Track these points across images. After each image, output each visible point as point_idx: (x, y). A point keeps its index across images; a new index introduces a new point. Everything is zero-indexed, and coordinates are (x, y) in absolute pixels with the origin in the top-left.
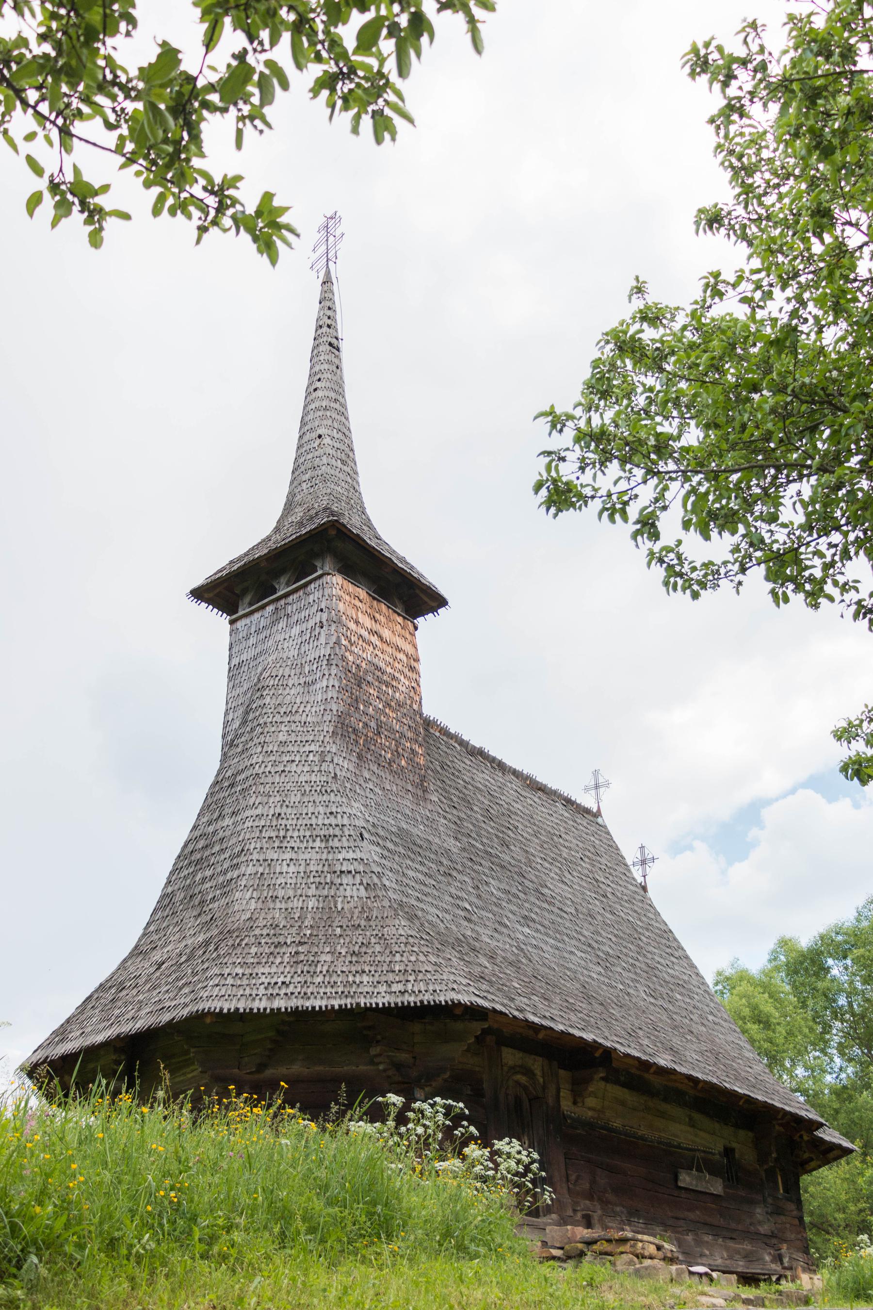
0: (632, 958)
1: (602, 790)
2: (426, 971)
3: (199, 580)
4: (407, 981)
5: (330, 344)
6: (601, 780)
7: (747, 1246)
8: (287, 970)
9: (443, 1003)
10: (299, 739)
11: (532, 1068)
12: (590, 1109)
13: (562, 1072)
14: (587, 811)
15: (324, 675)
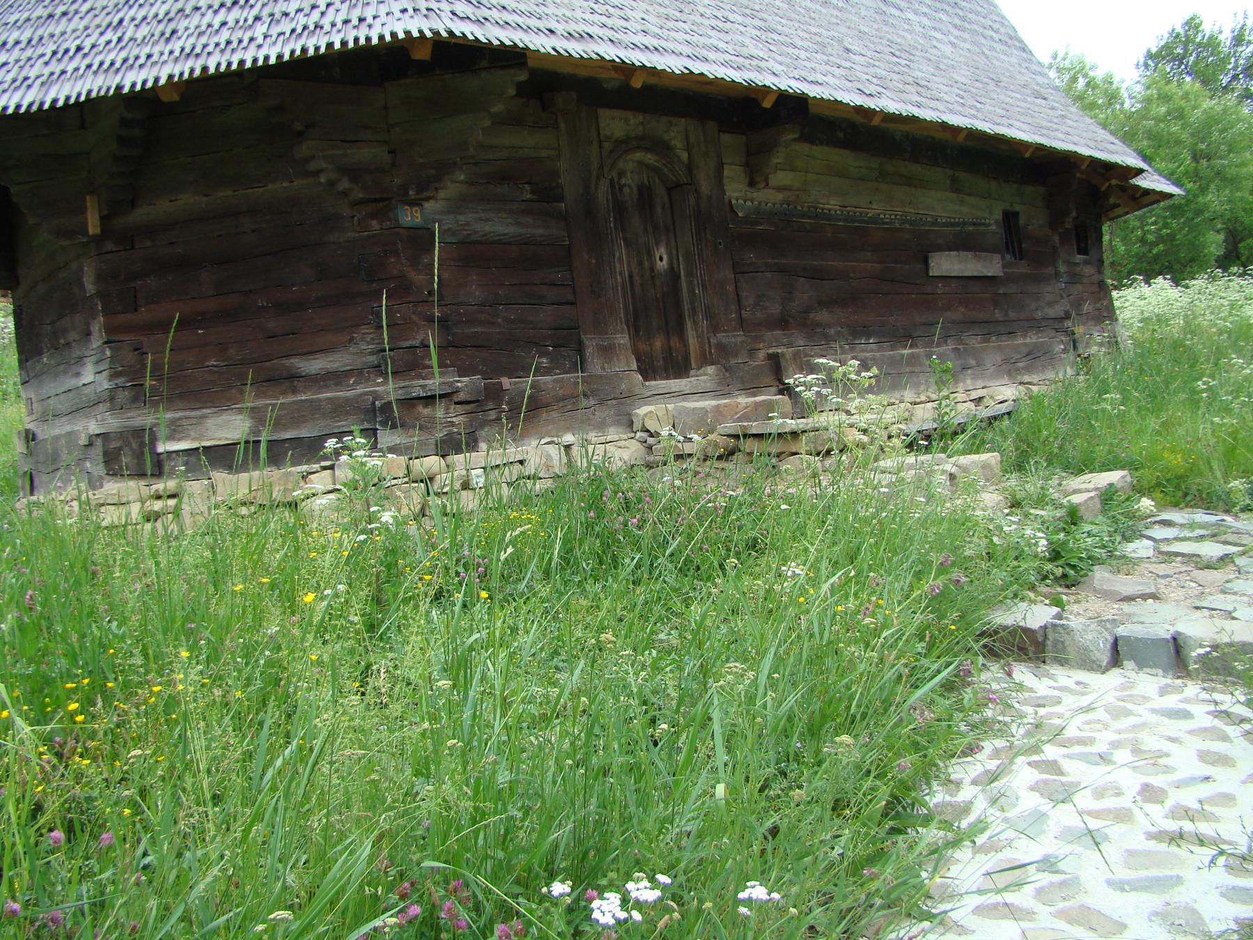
2: (428, 9)
7: (1032, 339)
11: (666, 137)
12: (779, 189)
13: (726, 138)
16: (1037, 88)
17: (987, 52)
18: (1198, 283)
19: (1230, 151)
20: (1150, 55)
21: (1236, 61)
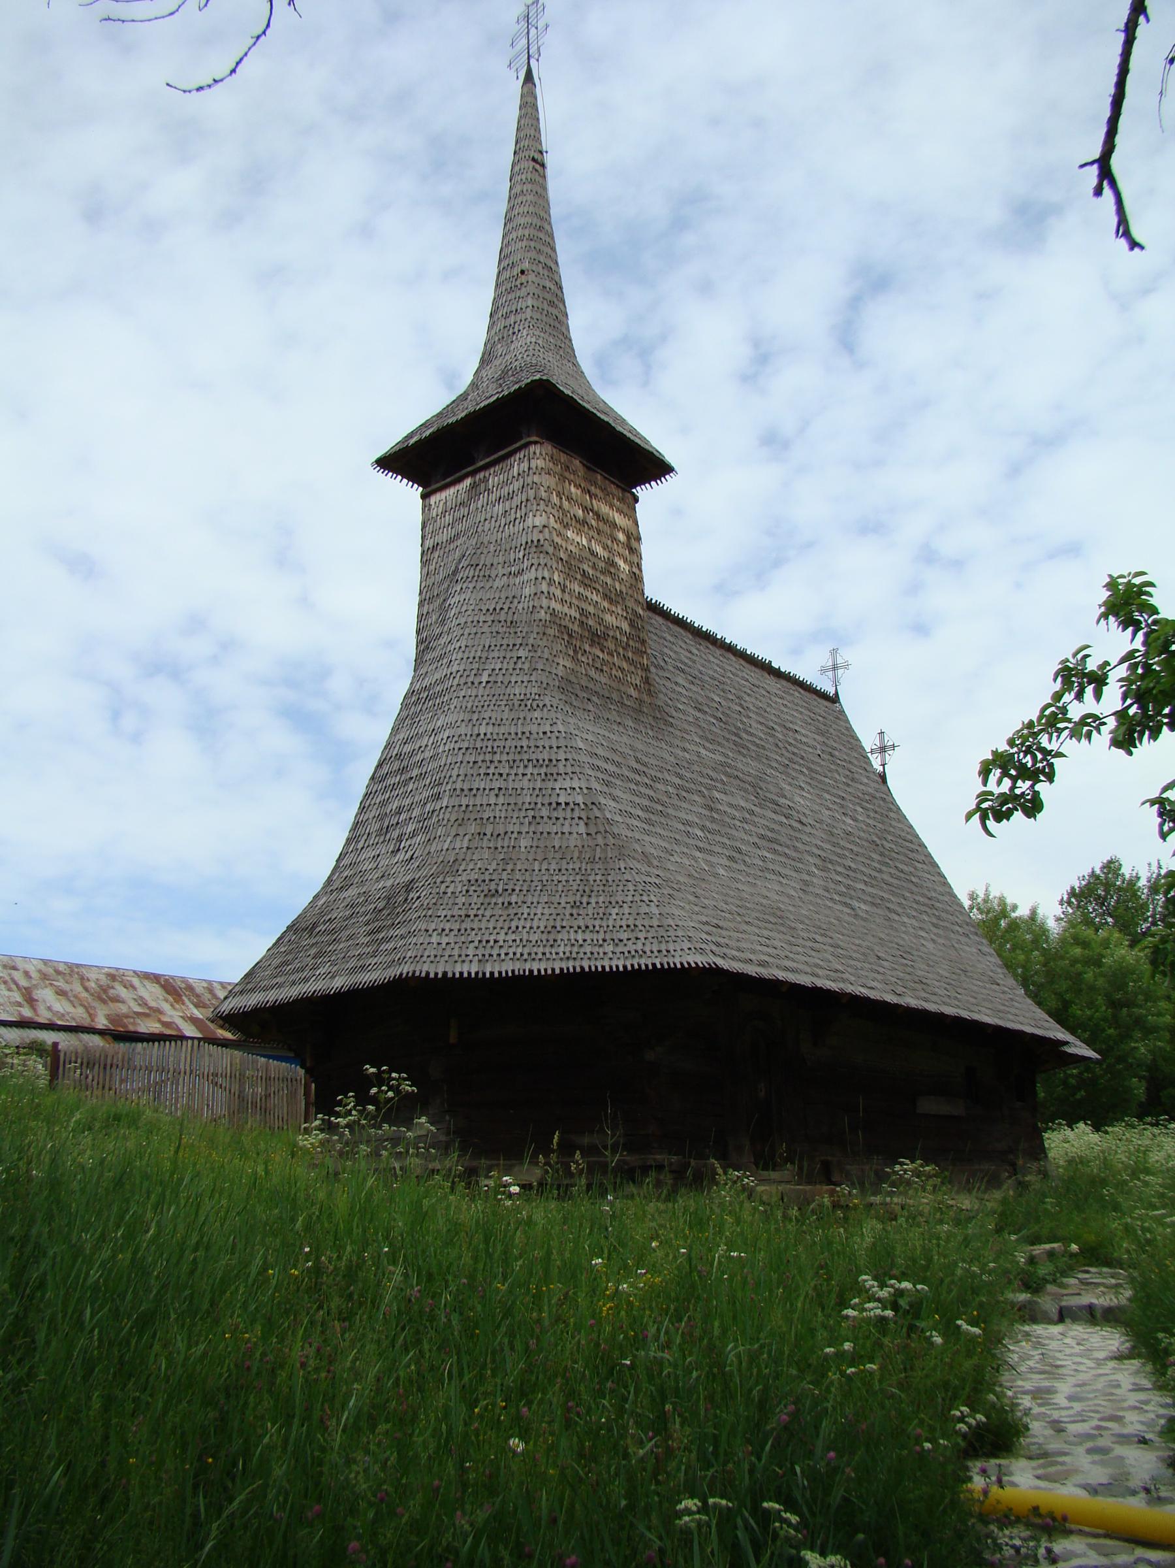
0: (875, 869)
1: (840, 672)
3: (385, 446)
4: (637, 939)
5: (534, 160)
6: (839, 661)
8: (499, 925)
9: (679, 966)
10: (505, 642)
14: (823, 696)
15: (532, 564)
16: (991, 974)
17: (956, 945)
18: (1117, 1129)
19: (1146, 1001)
20: (1072, 893)
21: (1154, 909)
